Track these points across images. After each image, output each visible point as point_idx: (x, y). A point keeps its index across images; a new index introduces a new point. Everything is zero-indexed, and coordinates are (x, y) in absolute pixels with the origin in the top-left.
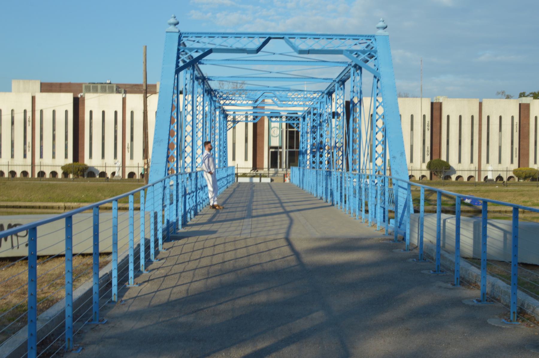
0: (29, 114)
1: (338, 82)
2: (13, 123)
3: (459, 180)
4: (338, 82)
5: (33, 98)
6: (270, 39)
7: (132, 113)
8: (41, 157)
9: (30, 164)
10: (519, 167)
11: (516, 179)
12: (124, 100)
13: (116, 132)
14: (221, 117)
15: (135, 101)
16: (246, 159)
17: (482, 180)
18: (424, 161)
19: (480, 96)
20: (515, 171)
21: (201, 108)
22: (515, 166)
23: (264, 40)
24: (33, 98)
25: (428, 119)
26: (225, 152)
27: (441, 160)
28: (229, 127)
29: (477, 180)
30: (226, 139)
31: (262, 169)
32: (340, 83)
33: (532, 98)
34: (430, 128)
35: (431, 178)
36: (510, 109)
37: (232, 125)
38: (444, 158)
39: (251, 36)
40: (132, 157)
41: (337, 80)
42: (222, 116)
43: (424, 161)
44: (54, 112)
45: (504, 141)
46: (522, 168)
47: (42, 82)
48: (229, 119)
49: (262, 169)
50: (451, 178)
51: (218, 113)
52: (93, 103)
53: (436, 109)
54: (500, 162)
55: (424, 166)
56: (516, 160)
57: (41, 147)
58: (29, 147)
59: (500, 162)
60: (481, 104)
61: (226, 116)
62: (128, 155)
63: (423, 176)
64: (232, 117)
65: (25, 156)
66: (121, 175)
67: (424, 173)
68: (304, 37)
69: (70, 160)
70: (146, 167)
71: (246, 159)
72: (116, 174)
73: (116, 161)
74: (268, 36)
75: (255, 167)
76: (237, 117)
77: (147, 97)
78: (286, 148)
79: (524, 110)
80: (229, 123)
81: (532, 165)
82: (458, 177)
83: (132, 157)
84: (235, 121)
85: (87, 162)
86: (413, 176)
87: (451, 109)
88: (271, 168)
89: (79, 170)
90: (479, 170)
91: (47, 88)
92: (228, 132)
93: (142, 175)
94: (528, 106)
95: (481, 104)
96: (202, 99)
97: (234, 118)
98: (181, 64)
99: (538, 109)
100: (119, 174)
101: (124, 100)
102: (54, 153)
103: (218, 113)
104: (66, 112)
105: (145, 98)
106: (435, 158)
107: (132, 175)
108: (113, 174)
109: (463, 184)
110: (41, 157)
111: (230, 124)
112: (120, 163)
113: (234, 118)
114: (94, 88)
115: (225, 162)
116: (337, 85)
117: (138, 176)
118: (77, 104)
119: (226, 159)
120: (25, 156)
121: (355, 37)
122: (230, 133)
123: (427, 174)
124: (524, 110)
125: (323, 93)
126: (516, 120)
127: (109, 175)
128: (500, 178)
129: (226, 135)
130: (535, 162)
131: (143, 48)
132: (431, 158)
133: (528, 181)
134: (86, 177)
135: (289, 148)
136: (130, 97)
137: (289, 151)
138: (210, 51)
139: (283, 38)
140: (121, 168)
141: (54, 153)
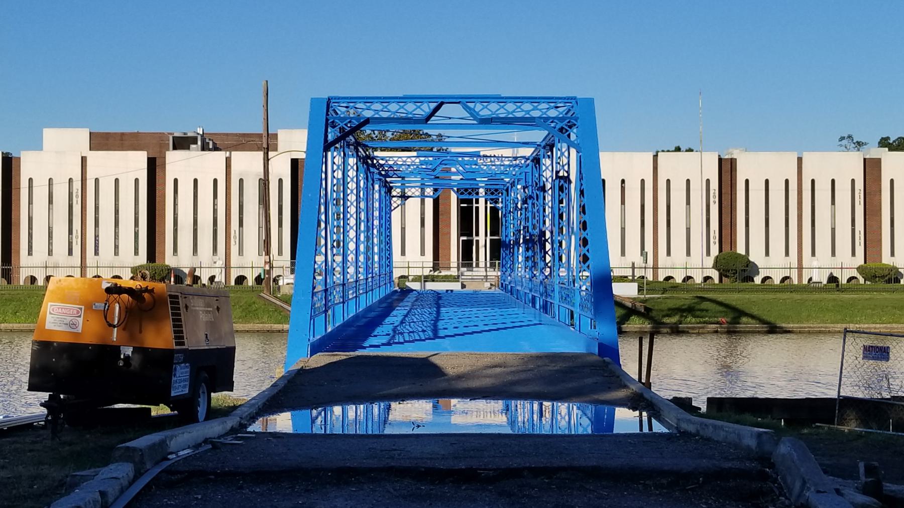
0: (77, 185)
1: (544, 147)
2: (51, 201)
3: (767, 282)
4: (544, 147)
5: (84, 160)
6: (442, 104)
7: (241, 181)
8: (96, 253)
9: (79, 265)
10: (865, 262)
11: (862, 281)
12: (228, 161)
13: (215, 211)
14: (383, 193)
15: (247, 163)
16: (423, 253)
17: (805, 282)
18: (708, 254)
19: (800, 144)
20: (859, 269)
21: (355, 185)
22: (859, 260)
23: (435, 105)
24: (84, 160)
25: (715, 185)
26: (389, 243)
27: (736, 253)
28: (395, 205)
29: (796, 282)
30: (390, 225)
31: (449, 268)
32: (548, 148)
33: (887, 149)
34: (717, 200)
35: (721, 280)
36: (850, 167)
37: (399, 202)
38: (741, 250)
39: (418, 99)
40: (241, 252)
41: (543, 144)
42: (383, 190)
43: (708, 254)
44: (117, 181)
45: (840, 218)
46: (870, 264)
47: (96, 130)
48: (394, 193)
49: (449, 268)
50: (753, 281)
51: (377, 187)
52: (179, 165)
53: (727, 169)
54: (833, 254)
55: (710, 262)
56: (860, 250)
57: (96, 237)
58: (77, 237)
59: (833, 254)
60: (800, 160)
61: (390, 189)
62: (234, 249)
63: (707, 279)
64: (399, 190)
65: (70, 253)
66: (223, 281)
67: (708, 273)
68: (485, 99)
69: (142, 259)
70: (267, 268)
71: (423, 253)
72: (216, 280)
73: (216, 258)
74: (440, 101)
75: (436, 267)
76: (406, 190)
77: (268, 160)
78: (486, 235)
79: (872, 168)
80: (394, 199)
81: (886, 259)
82: (766, 278)
83: (241, 252)
84: (404, 197)
85: (170, 260)
86: (672, 278)
87: (752, 168)
88: (463, 266)
89: (735, 268)
90: (800, 268)
91: (101, 141)
92: (393, 213)
93: (259, 280)
94: (878, 162)
95: (800, 160)
96: (355, 173)
97: (403, 192)
98: (330, 137)
99: (894, 164)
100: (220, 278)
101: (228, 161)
102: (116, 247)
103: (377, 187)
104: (137, 181)
105: (267, 160)
106: (726, 248)
107: (241, 280)
108: (212, 279)
109: (675, 287)
110: (96, 253)
111: (396, 202)
112: (221, 263)
113: (403, 192)
114: (182, 143)
115: (389, 258)
116: (541, 153)
117: (250, 282)
118: (154, 168)
119: (390, 254)
120: (70, 253)
121: (551, 100)
122: (396, 215)
123: (715, 275)
124: (872, 168)
125: (528, 159)
126: (860, 185)
127: (205, 280)
128: (832, 279)
129: (390, 217)
130: (893, 254)
131: (264, 83)
132: (721, 250)
133: (881, 285)
134: (763, 274)
135: (491, 235)
136: (238, 157)
137: (491, 240)
138: (367, 121)
139: (459, 103)
140: (224, 270)
141: (116, 247)
